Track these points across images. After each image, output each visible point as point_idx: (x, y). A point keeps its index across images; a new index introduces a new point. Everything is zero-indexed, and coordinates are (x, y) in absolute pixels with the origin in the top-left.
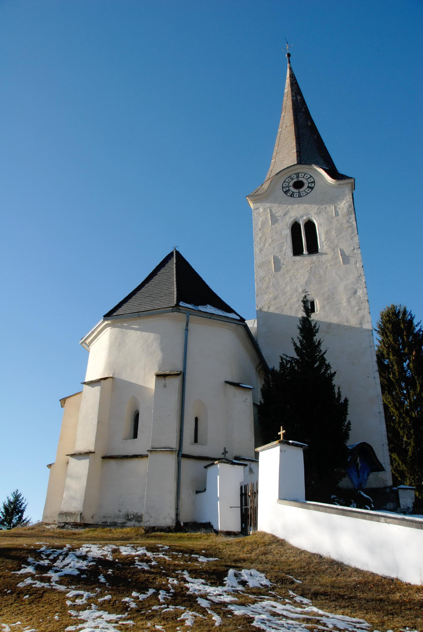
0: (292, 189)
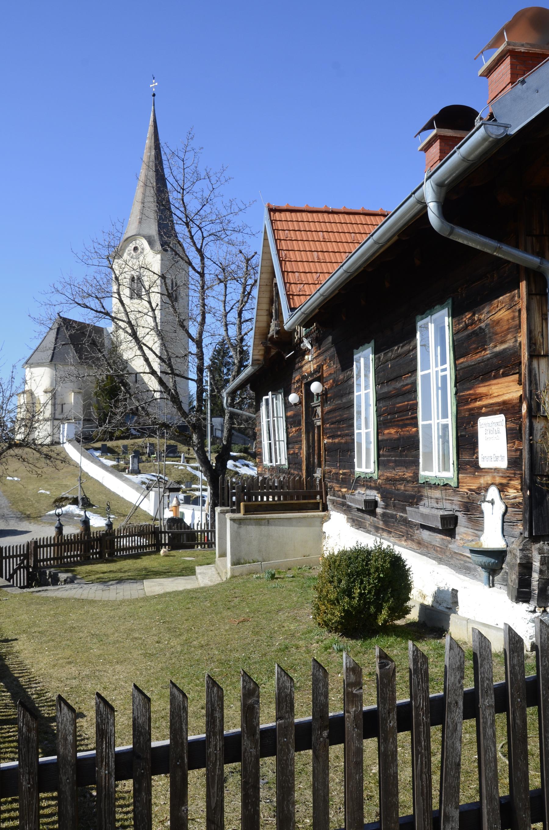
0: (132, 252)
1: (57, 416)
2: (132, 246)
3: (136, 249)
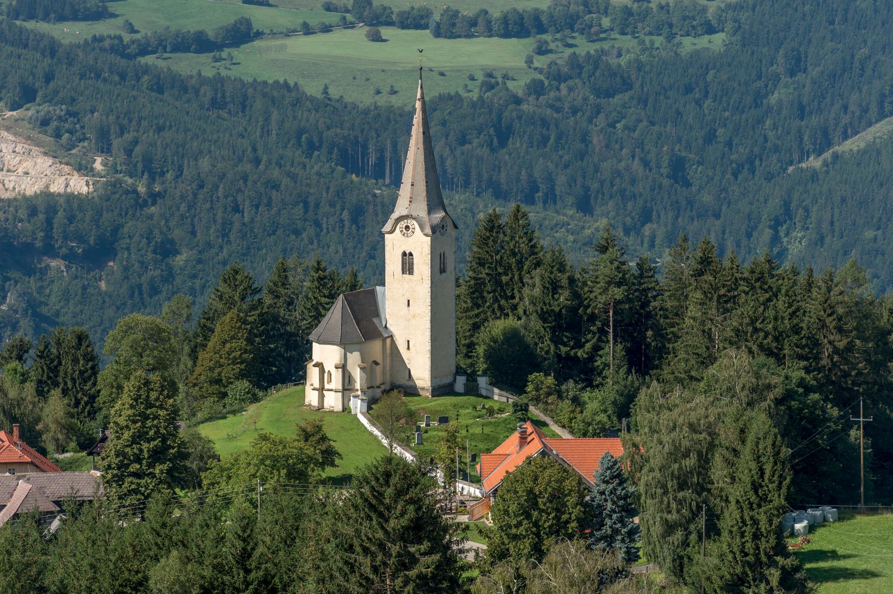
1: (346, 387)
2: (403, 224)
3: (407, 227)
